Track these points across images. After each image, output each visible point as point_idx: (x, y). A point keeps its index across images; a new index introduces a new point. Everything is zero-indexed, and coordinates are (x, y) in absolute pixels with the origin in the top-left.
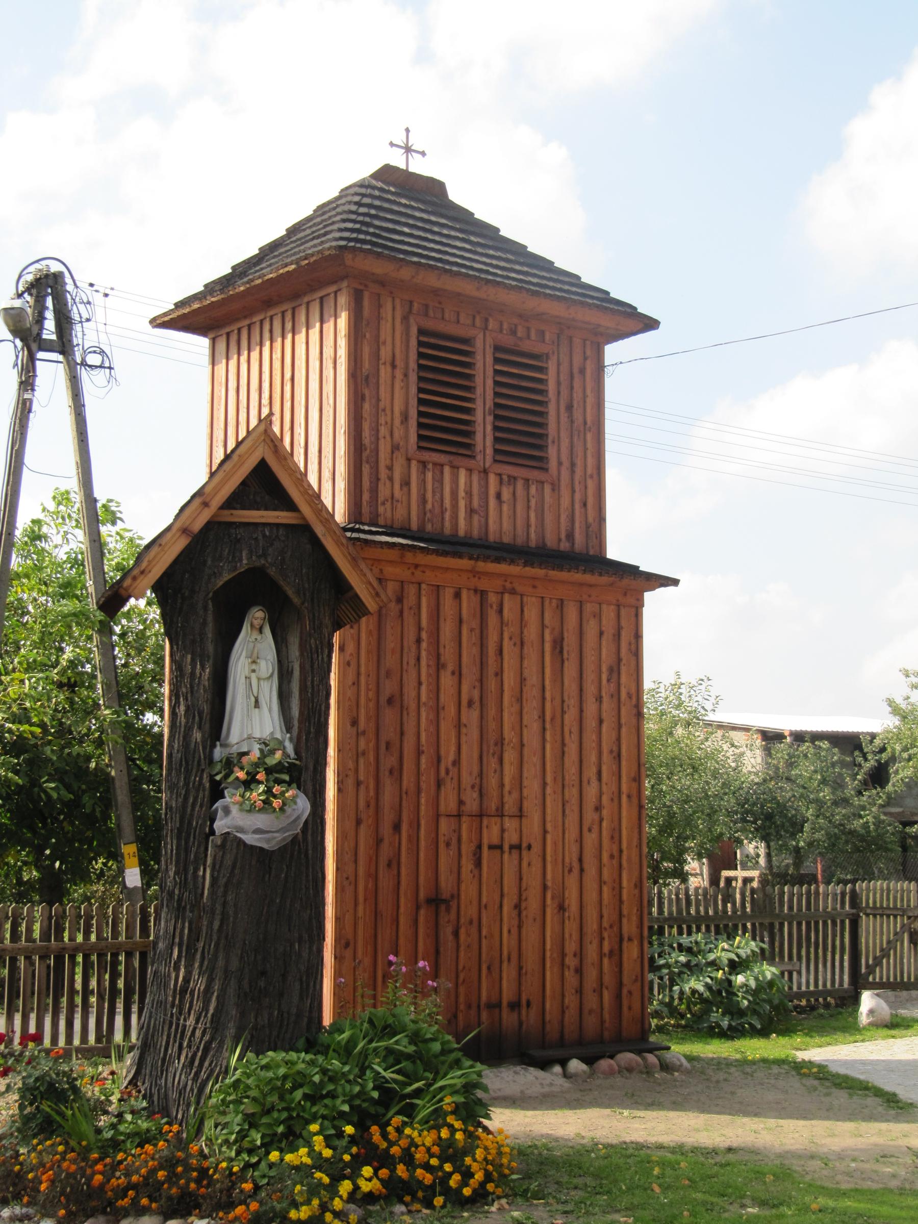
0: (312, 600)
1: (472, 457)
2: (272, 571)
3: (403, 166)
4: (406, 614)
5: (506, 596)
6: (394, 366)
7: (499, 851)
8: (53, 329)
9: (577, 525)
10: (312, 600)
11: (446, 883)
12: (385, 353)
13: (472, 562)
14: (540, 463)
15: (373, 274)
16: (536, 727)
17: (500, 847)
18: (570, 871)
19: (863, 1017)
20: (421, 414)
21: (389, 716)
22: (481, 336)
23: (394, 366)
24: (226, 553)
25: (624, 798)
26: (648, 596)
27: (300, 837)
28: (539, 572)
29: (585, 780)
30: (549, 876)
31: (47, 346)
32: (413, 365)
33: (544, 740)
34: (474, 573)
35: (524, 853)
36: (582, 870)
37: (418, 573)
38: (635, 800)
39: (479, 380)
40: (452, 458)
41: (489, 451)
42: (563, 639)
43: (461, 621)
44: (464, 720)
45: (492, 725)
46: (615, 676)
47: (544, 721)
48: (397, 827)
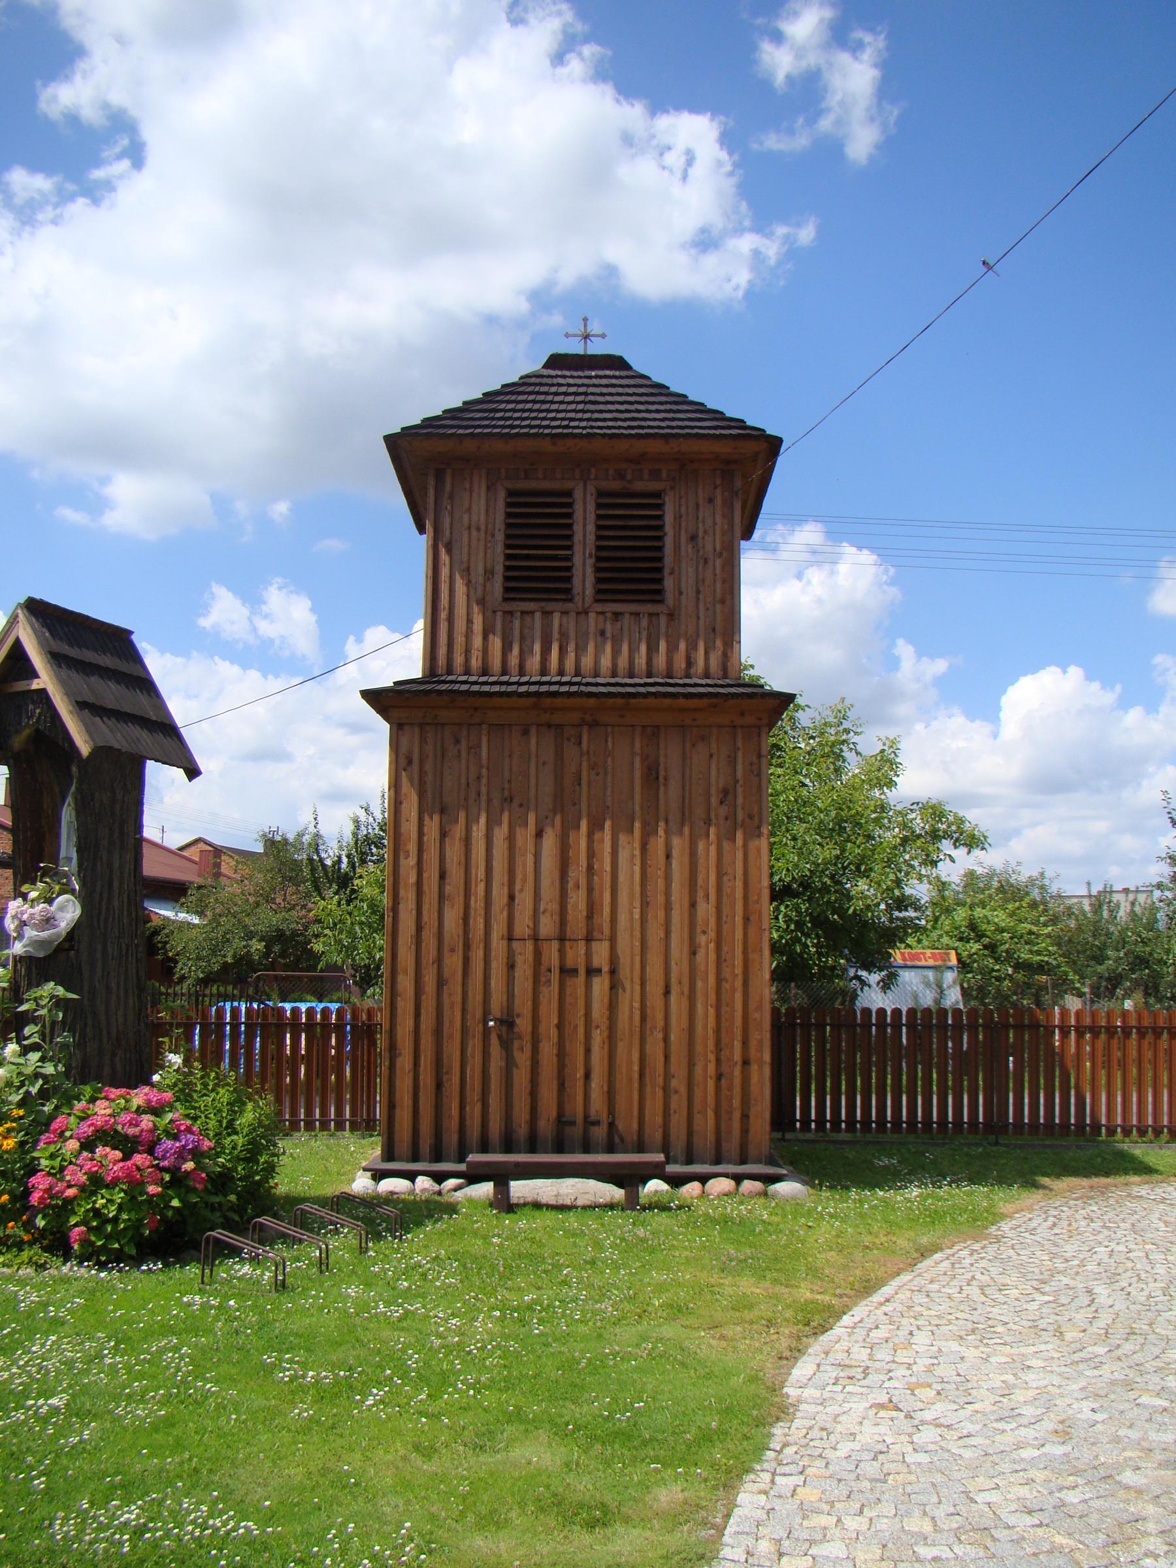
40: (543, 604)
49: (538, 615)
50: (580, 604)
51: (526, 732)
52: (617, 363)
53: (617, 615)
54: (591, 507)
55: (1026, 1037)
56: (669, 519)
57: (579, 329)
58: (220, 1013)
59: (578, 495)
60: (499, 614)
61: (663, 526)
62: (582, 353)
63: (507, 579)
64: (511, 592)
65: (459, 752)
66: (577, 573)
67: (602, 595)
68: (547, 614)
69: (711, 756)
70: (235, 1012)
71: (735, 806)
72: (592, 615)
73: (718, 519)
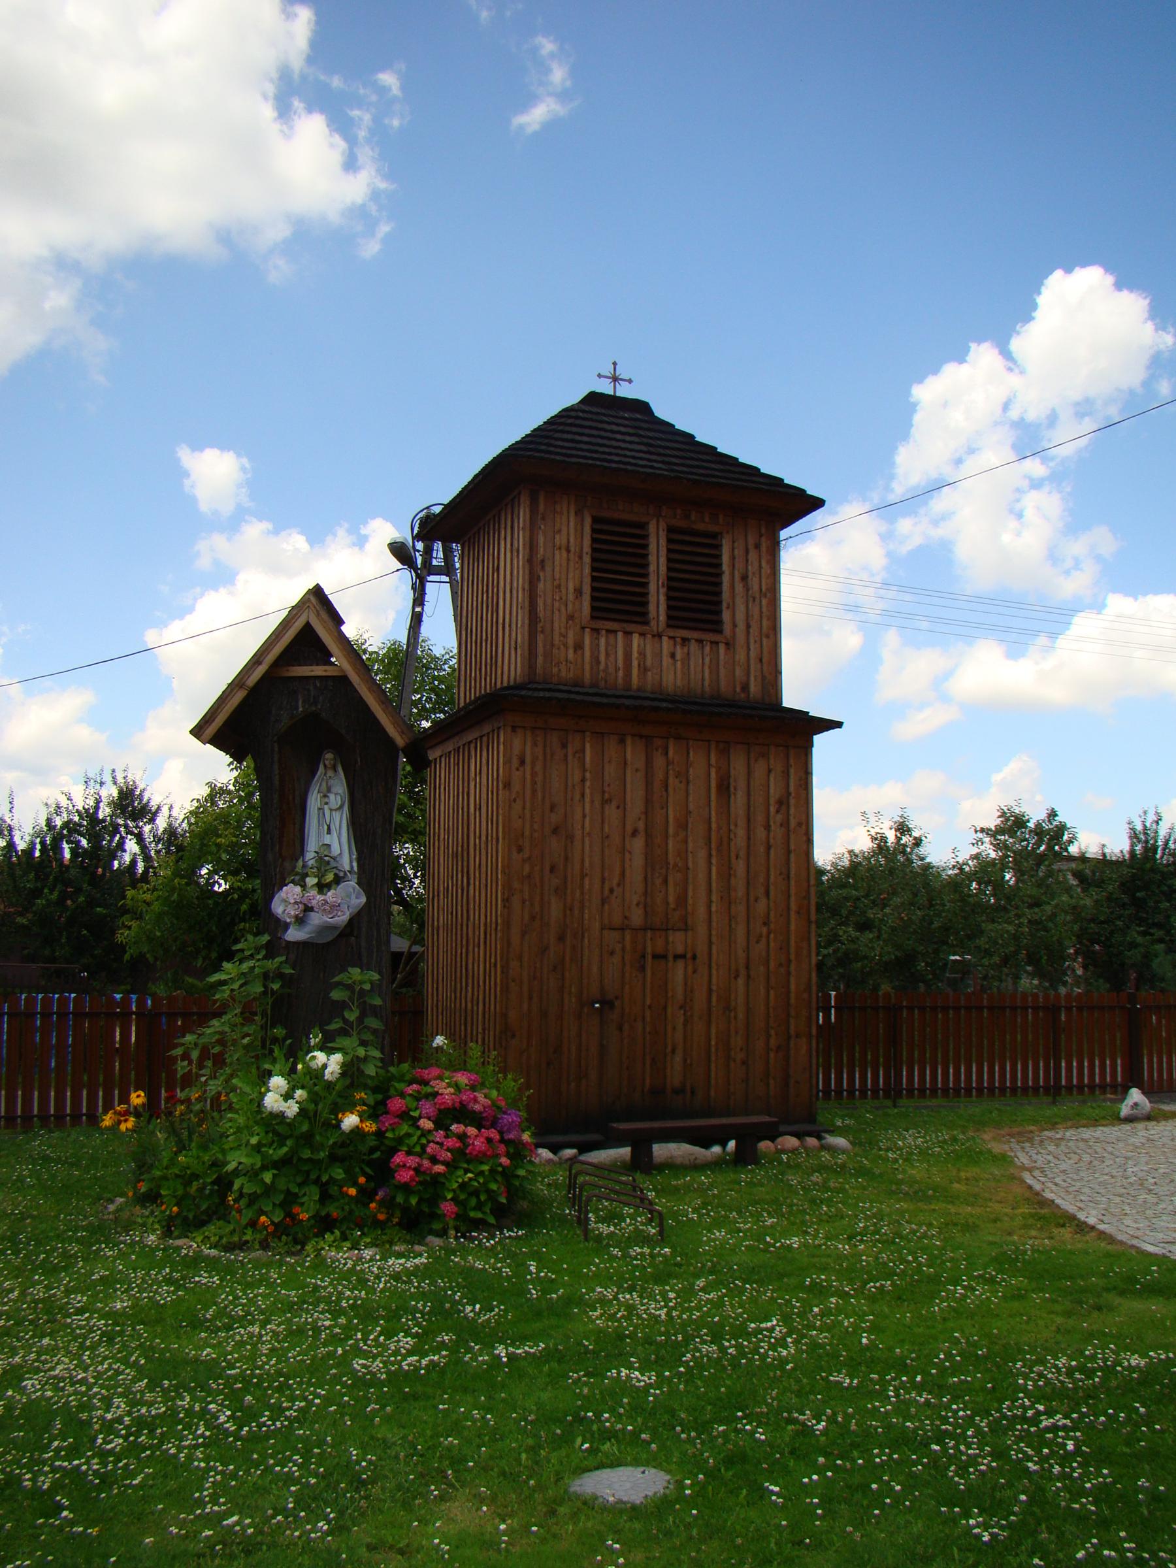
1: (646, 623)
4: (570, 757)
6: (568, 551)
8: (441, 555)
9: (752, 679)
17: (665, 957)
19: (1125, 1110)
23: (568, 551)
26: (817, 739)
30: (714, 980)
31: (438, 571)
33: (710, 863)
36: (748, 976)
40: (625, 625)
41: (663, 618)
43: (625, 763)
44: (628, 846)
46: (784, 808)
47: (710, 849)
49: (620, 634)
50: (655, 629)
51: (622, 741)
52: (642, 408)
53: (685, 641)
54: (663, 542)
55: (940, 1016)
56: (725, 558)
57: (608, 370)
58: (31, 1001)
59: (652, 528)
60: (587, 630)
61: (647, 555)
62: (612, 393)
63: (593, 599)
64: (597, 612)
65: (566, 756)
66: (652, 599)
67: (675, 620)
68: (628, 634)
69: (770, 771)
70: (63, 1002)
71: (788, 815)
72: (665, 639)
73: (764, 564)
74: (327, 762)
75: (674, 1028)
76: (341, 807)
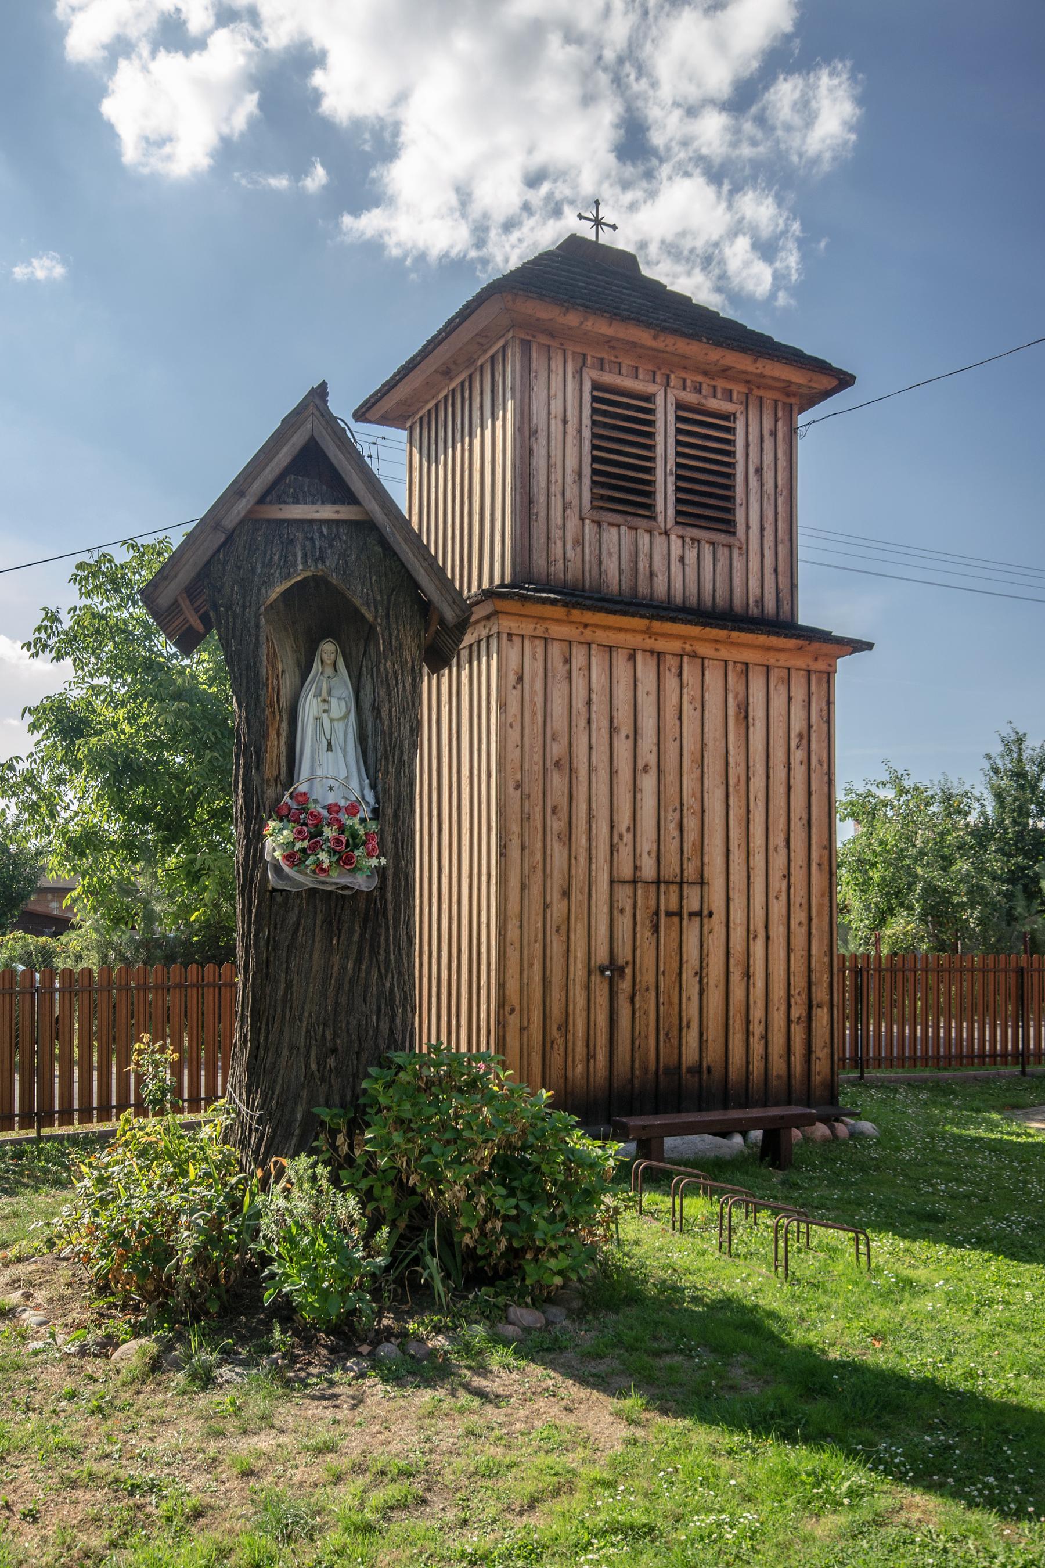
0: (388, 615)
2: (334, 579)
3: (592, 237)
5: (686, 659)
6: (565, 422)
7: (698, 919)
10: (388, 615)
11: (624, 954)
12: (556, 406)
13: (646, 622)
14: (727, 526)
15: (538, 320)
16: (719, 793)
17: (679, 914)
18: (755, 937)
20: (594, 472)
21: (558, 781)
22: (662, 392)
24: (276, 557)
25: (814, 867)
27: (377, 893)
28: (722, 634)
29: (771, 847)
32: (587, 421)
34: (648, 632)
35: (706, 920)
36: (768, 938)
37: (588, 632)
38: (826, 867)
39: (660, 438)
40: (629, 518)
41: (671, 512)
42: (748, 704)
45: (672, 791)
48: (566, 894)
50: (662, 525)
74: (325, 657)
75: (689, 998)
76: (347, 715)
